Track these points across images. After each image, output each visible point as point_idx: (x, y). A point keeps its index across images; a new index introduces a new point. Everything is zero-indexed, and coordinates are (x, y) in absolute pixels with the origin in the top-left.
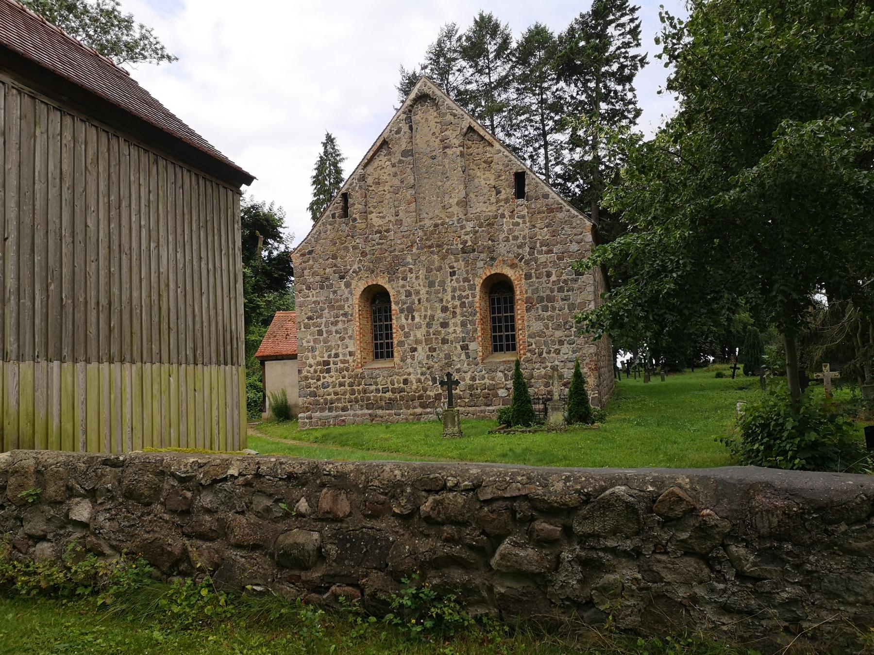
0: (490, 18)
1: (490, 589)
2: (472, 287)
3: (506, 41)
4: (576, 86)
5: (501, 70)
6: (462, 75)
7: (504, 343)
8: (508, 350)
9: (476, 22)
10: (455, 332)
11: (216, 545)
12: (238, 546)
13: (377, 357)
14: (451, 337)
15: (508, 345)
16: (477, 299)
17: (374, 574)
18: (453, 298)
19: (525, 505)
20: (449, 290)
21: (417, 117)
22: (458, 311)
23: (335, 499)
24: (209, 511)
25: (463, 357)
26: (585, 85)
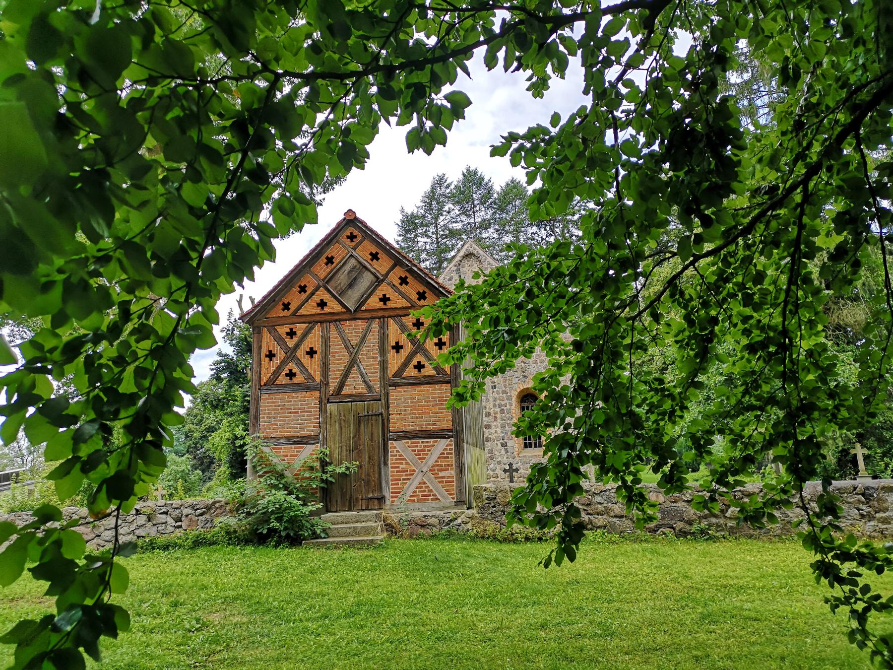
0: (476, 172)
1: (726, 525)
2: (509, 398)
3: (490, 191)
4: (545, 230)
5: (483, 214)
6: (452, 217)
7: (533, 441)
8: (536, 446)
9: (464, 174)
10: (496, 432)
11: (605, 516)
12: (615, 516)
13: (526, 447)
14: (493, 437)
15: (535, 443)
16: (513, 407)
17: (678, 523)
18: (495, 406)
19: (740, 493)
20: (491, 399)
21: (465, 269)
22: (498, 416)
23: (657, 496)
24: (600, 503)
25: (503, 452)
26: (552, 229)
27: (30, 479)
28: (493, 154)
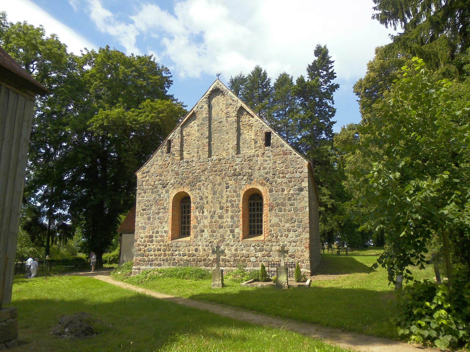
2: (238, 196)
14: (224, 225)
22: (229, 209)
25: (231, 237)
27: (321, 63)
28: (107, 46)
